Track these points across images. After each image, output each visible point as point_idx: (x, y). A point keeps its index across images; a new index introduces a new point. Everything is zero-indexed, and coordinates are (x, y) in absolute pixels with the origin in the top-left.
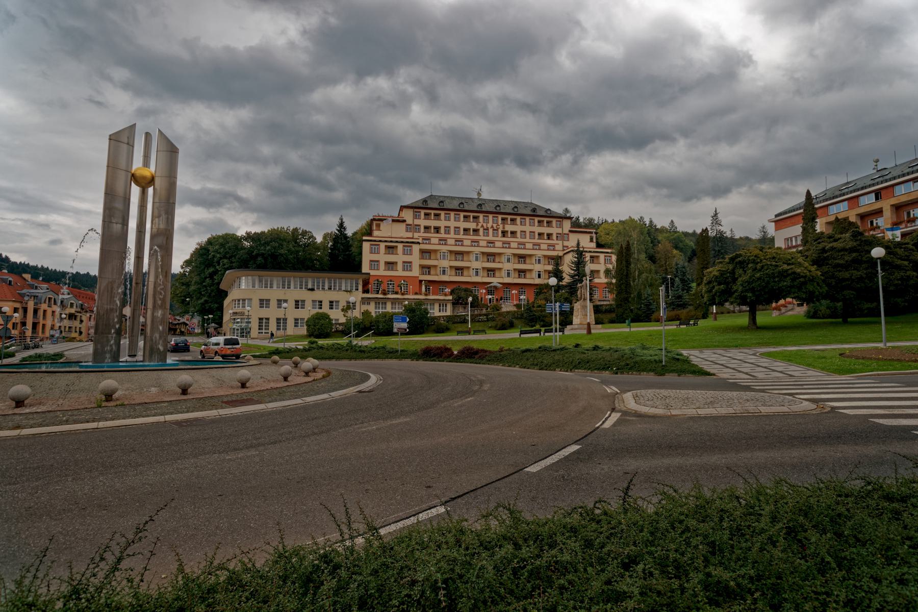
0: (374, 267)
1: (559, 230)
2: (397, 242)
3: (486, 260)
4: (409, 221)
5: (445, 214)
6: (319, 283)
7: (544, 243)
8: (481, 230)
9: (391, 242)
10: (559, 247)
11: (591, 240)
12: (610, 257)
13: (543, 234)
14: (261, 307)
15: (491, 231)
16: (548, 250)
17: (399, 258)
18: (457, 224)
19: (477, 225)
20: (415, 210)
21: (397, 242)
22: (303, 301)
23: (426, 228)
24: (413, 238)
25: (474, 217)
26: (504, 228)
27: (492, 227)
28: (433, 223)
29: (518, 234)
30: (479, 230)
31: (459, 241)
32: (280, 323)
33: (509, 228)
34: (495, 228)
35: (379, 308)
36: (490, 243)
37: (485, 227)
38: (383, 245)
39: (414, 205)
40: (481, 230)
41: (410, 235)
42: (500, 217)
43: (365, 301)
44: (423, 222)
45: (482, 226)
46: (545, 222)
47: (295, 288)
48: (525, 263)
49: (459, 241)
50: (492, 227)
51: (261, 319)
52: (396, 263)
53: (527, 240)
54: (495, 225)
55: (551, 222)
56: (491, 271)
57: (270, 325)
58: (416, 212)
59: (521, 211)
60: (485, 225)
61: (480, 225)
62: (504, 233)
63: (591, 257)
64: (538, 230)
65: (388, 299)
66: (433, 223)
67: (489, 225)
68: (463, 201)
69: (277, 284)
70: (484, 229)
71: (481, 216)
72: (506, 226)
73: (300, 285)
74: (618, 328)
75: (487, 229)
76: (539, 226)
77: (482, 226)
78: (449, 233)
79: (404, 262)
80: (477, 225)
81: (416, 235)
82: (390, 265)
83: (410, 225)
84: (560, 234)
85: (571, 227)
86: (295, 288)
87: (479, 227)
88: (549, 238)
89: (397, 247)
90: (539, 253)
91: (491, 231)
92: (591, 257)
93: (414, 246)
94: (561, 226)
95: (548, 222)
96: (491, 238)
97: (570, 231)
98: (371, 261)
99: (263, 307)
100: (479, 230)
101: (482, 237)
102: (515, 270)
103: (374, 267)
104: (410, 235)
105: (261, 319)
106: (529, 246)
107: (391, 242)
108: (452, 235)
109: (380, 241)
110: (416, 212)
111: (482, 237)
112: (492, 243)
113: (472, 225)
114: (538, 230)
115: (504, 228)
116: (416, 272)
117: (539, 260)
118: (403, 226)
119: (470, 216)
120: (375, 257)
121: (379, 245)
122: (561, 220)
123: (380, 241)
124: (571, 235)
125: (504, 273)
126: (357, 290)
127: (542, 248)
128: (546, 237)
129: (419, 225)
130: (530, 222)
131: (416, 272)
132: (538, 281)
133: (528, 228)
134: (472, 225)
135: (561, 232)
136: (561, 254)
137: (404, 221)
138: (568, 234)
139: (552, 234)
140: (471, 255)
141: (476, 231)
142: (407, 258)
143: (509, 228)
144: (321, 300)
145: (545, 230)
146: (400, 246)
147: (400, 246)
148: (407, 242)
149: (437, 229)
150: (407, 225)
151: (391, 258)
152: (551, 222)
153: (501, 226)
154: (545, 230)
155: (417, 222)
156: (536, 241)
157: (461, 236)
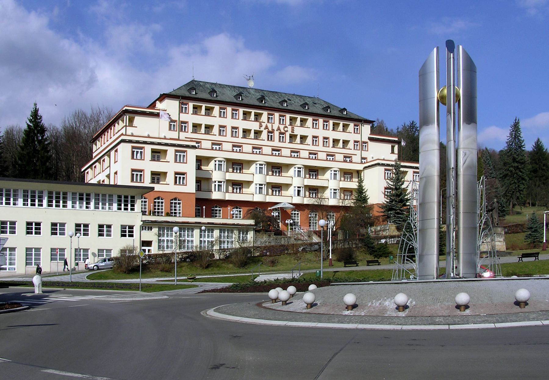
1: (357, 137)
2: (166, 145)
7: (339, 151)
9: (159, 144)
10: (356, 159)
11: (393, 152)
12: (184, 152)
13: (200, 125)
14: (53, 234)
15: (277, 134)
16: (345, 161)
18: (235, 123)
19: (261, 126)
21: (166, 145)
22: (63, 225)
24: (178, 139)
26: (293, 131)
27: (279, 129)
31: (237, 146)
33: (299, 131)
34: (282, 131)
35: (205, 236)
37: (270, 129)
38: (148, 149)
39: (174, 93)
41: (175, 135)
42: (288, 116)
43: (147, 226)
44: (190, 118)
45: (267, 128)
49: (237, 146)
50: (279, 129)
52: (165, 174)
53: (320, 148)
54: (282, 127)
56: (277, 188)
59: (312, 110)
60: (269, 126)
61: (264, 125)
62: (293, 137)
63: (154, 151)
64: (242, 125)
67: (275, 127)
68: (241, 91)
69: (95, 204)
70: (269, 132)
71: (265, 114)
72: (295, 128)
73: (32, 201)
75: (272, 132)
76: (245, 119)
77: (267, 128)
79: (176, 173)
80: (261, 126)
81: (183, 135)
82: (157, 177)
87: (262, 129)
88: (256, 138)
89: (166, 151)
91: (277, 134)
93: (189, 150)
96: (276, 143)
97: (371, 139)
98: (133, 170)
99: (32, 233)
101: (266, 143)
104: (175, 135)
106: (322, 156)
107: (159, 144)
108: (229, 138)
109: (145, 143)
113: (253, 126)
114: (242, 125)
115: (293, 131)
116: (190, 187)
117: (220, 165)
120: (137, 164)
121: (184, 152)
123: (145, 143)
124: (371, 144)
126: (42, 205)
127: (354, 160)
128: (203, 130)
132: (258, 198)
133: (229, 122)
134: (253, 126)
135: (360, 140)
136: (360, 167)
141: (258, 133)
142: (180, 168)
144: (86, 222)
145: (341, 136)
146: (171, 151)
147: (171, 151)
148: (138, 142)
149: (209, 128)
151: (158, 167)
152: (306, 120)
154: (341, 136)
155: (184, 117)
156: (331, 150)
157: (240, 140)
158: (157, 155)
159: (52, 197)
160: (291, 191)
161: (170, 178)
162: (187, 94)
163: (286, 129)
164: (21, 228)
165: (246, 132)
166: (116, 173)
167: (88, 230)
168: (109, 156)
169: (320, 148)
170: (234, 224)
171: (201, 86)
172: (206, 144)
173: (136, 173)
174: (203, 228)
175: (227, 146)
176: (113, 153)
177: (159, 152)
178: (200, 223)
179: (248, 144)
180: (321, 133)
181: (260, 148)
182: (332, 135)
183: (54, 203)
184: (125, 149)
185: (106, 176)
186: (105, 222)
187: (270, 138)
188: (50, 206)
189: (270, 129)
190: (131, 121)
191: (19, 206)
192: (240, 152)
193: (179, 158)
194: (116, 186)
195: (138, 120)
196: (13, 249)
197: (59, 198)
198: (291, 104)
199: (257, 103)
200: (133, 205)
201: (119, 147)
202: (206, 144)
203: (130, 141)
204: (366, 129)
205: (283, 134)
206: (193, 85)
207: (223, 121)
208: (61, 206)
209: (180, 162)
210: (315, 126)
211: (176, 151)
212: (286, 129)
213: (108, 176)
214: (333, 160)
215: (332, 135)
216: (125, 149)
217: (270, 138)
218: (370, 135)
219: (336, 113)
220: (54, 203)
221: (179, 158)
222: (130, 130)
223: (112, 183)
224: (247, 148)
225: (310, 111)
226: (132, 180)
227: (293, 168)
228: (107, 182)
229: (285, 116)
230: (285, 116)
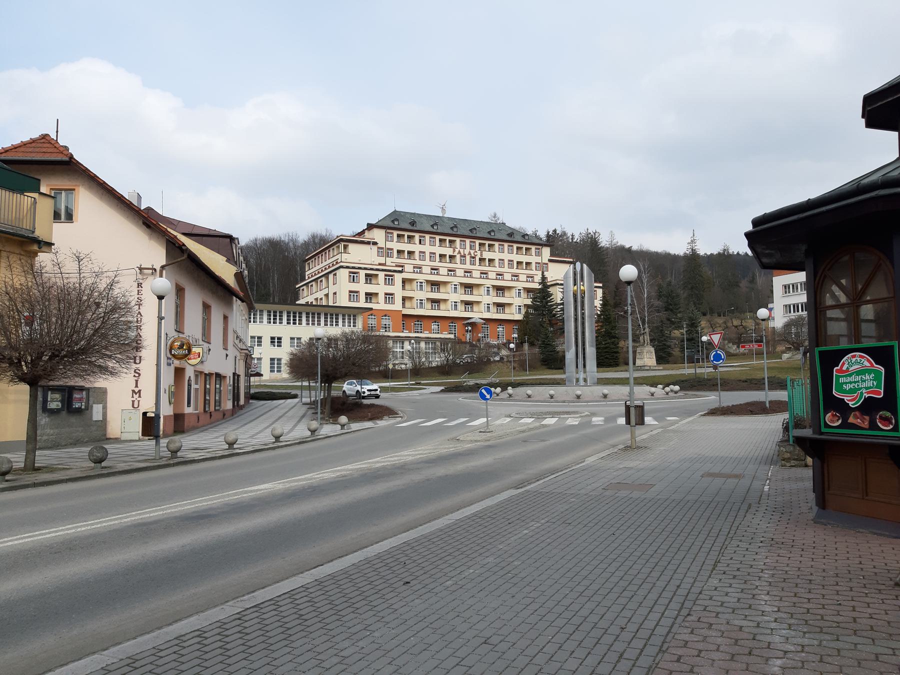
0: (354, 299)
1: (539, 259)
3: (430, 290)
4: (381, 244)
5: (536, 249)
6: (333, 318)
7: (523, 273)
8: (458, 257)
13: (403, 251)
15: (468, 258)
17: (380, 288)
19: (454, 251)
20: (388, 231)
23: (400, 252)
25: (450, 241)
26: (481, 255)
27: (470, 254)
28: (406, 247)
29: (417, 255)
30: (455, 256)
32: (274, 364)
33: (487, 255)
34: (473, 255)
36: (450, 271)
37: (462, 254)
38: (362, 273)
39: (380, 224)
40: (458, 257)
44: (395, 245)
45: (459, 252)
46: (487, 245)
47: (288, 323)
48: (439, 291)
50: (470, 254)
51: (272, 360)
52: (377, 294)
54: (472, 252)
55: (530, 249)
57: (269, 366)
58: (388, 233)
59: (498, 236)
60: (462, 251)
61: (457, 251)
62: (482, 260)
63: (367, 275)
64: (439, 250)
65: (389, 336)
66: (406, 247)
68: (436, 221)
70: (461, 256)
71: (458, 240)
74: (552, 374)
75: (464, 256)
77: (459, 252)
78: (474, 264)
79: (386, 294)
80: (454, 251)
81: (389, 261)
82: (370, 296)
83: (382, 248)
84: (539, 263)
85: (550, 257)
86: (288, 323)
90: (421, 278)
91: (468, 258)
92: (367, 275)
94: (539, 254)
95: (409, 237)
96: (468, 266)
97: (550, 261)
98: (350, 292)
100: (455, 256)
101: (459, 266)
102: (462, 301)
103: (354, 299)
105: (272, 360)
108: (427, 262)
110: (388, 233)
111: (459, 266)
112: (516, 276)
113: (448, 251)
114: (439, 250)
115: (481, 255)
118: (375, 248)
119: (404, 235)
120: (354, 287)
121: (392, 276)
122: (540, 247)
124: (550, 264)
125: (482, 307)
126: (262, 322)
129: (392, 249)
130: (430, 241)
131: (397, 306)
134: (448, 251)
137: (375, 243)
138: (547, 264)
139: (414, 252)
140: (449, 286)
142: (389, 289)
143: (487, 255)
145: (524, 259)
146: (381, 275)
148: (354, 268)
149: (411, 253)
150: (379, 248)
151: (371, 288)
153: (479, 252)
154: (524, 259)
155: (390, 245)
156: (515, 271)
158: (369, 278)
159: (270, 315)
160: (482, 307)
161: (381, 297)
162: (392, 225)
163: (476, 254)
164: (266, 341)
165: (442, 256)
166: (335, 293)
167: (261, 342)
168: (328, 279)
169: (506, 269)
170: (436, 338)
171: (402, 216)
172: (409, 268)
173: (353, 294)
174: (413, 341)
175: (427, 270)
176: (331, 276)
177: (371, 276)
178: (409, 337)
179: (477, 269)
180: (506, 256)
181: (454, 271)
182: (516, 258)
183: (278, 321)
184: (343, 274)
185: (325, 295)
186: (276, 335)
187: (463, 262)
188: (308, 324)
189: (462, 254)
190: (345, 247)
191: (284, 324)
192: (420, 273)
193: (389, 280)
194: (328, 306)
195: (351, 247)
196: (259, 359)
197: (276, 316)
198: (479, 231)
199: (450, 232)
200: (354, 323)
201: (337, 272)
202: (409, 268)
203: (347, 267)
204: (546, 252)
205: (473, 258)
206: (396, 216)
207: (502, 256)
208: (272, 322)
209: (389, 284)
210: (433, 244)
211: (386, 275)
212: (476, 254)
213: (327, 295)
214: (518, 280)
215: (516, 258)
216: (343, 274)
217: (463, 262)
218: (550, 257)
219: (520, 239)
220: (278, 321)
221: (389, 280)
222: (345, 256)
223: (331, 304)
224: (443, 271)
225: (495, 237)
226: (350, 300)
227: (415, 282)
228: (314, 303)
229: (393, 233)
230: (435, 238)
